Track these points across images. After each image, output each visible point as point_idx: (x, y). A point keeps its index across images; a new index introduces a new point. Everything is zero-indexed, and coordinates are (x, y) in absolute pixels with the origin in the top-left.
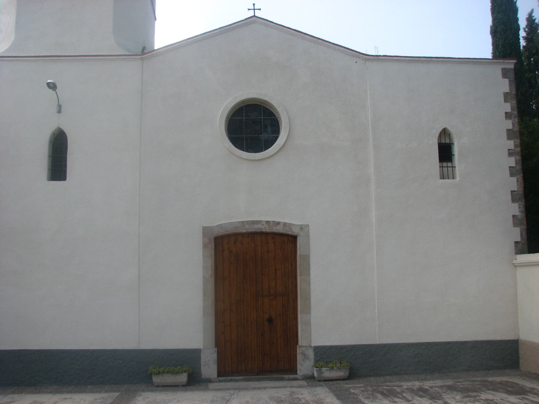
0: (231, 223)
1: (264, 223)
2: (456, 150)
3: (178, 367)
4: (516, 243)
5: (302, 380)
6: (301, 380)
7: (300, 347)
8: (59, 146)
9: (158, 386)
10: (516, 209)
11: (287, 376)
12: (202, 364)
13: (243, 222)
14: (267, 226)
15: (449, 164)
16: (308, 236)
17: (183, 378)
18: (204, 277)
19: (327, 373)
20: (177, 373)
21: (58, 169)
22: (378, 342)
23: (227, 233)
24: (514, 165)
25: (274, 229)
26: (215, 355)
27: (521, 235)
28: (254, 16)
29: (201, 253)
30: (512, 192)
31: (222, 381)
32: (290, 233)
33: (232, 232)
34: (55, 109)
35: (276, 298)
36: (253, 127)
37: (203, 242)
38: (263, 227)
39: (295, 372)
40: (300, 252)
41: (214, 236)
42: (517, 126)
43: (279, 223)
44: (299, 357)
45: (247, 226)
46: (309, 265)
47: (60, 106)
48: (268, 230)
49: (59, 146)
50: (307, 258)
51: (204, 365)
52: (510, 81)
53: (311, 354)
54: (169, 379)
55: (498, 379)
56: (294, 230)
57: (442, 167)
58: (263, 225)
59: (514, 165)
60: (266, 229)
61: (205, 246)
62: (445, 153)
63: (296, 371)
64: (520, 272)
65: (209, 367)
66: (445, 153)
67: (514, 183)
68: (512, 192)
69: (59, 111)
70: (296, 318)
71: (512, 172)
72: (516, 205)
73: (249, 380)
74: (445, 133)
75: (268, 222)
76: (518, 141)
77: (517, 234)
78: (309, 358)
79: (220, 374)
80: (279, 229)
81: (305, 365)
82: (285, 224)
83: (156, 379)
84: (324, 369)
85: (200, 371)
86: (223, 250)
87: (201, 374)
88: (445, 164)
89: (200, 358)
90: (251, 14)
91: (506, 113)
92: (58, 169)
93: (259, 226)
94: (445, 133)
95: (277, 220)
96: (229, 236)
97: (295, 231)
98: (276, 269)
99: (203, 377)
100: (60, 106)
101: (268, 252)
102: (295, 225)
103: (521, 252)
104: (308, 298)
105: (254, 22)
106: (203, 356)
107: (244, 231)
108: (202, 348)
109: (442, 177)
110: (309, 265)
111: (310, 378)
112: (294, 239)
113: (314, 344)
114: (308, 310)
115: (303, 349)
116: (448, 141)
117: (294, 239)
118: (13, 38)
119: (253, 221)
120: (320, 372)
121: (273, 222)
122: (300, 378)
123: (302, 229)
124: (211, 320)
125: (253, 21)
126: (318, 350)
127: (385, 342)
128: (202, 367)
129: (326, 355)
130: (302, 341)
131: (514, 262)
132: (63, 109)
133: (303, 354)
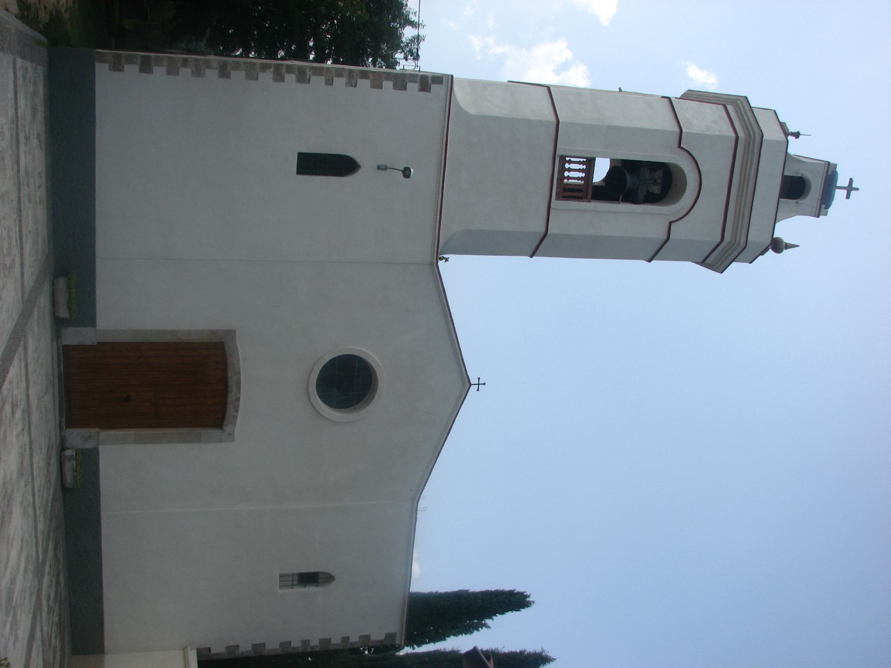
2: (311, 589)
3: (70, 260)
4: (209, 649)
7: (98, 433)
8: (340, 166)
9: (53, 284)
10: (245, 648)
11: (64, 419)
12: (78, 329)
13: (239, 373)
15: (295, 582)
16: (221, 441)
17: (63, 313)
18: (179, 331)
19: (69, 466)
20: (70, 309)
21: (313, 164)
22: (102, 513)
24: (292, 645)
26: (88, 343)
27: (217, 654)
28: (471, 385)
29: (206, 328)
30: (264, 645)
31: (58, 350)
32: (226, 423)
34: (382, 163)
36: (347, 382)
37: (218, 331)
39: (68, 427)
40: (204, 431)
43: (237, 411)
44: (85, 432)
47: (385, 168)
48: (229, 399)
49: (340, 166)
50: (197, 439)
52: (382, 641)
53: (90, 445)
54: (62, 298)
55: (66, 643)
57: (293, 575)
59: (292, 645)
60: (231, 397)
61: (213, 332)
62: (309, 579)
64: (179, 654)
65: (74, 336)
66: (309, 579)
67: (273, 645)
68: (264, 645)
69: (379, 168)
70: (129, 426)
71: (305, 642)
72: (250, 648)
73: (59, 380)
74: (329, 578)
75: (238, 399)
76: (318, 649)
77: (219, 649)
79: (65, 347)
80: (230, 411)
81: (77, 437)
82: (236, 417)
83: (61, 282)
84: (74, 463)
88: (296, 578)
89: (85, 326)
90: (473, 380)
91: (348, 638)
92: (313, 164)
93: (234, 391)
94: (329, 578)
95: (240, 409)
96: (224, 355)
97: (228, 428)
100: (385, 168)
103: (200, 653)
105: (464, 384)
106: (87, 329)
107: (229, 374)
109: (281, 576)
111: (63, 447)
113: (101, 448)
114: (139, 441)
116: (321, 580)
118: (472, 111)
120: (71, 458)
121: (238, 406)
123: (230, 434)
124: (129, 339)
125: (465, 384)
126: (95, 452)
127: (102, 521)
129: (88, 462)
130: (104, 434)
131: (189, 648)
132: (382, 172)
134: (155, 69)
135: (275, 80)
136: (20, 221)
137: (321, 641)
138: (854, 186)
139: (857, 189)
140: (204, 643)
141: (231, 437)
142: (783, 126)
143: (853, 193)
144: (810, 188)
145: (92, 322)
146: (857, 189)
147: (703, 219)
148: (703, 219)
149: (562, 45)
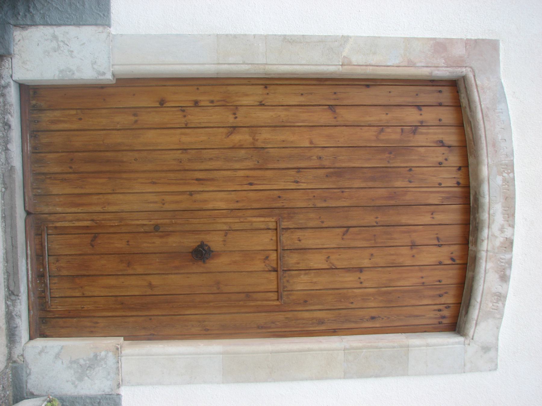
0: (507, 128)
1: (508, 233)
5: (10, 358)
6: (10, 353)
7: (117, 350)
12: (59, 31)
14: (497, 243)
18: (345, 39)
23: (479, 116)
25: (490, 265)
33: (482, 132)
35: (276, 270)
37: (451, 41)
38: (495, 228)
41: (471, 75)
42: (12, 31)
43: (504, 278)
45: (499, 180)
46: (379, 374)
50: (399, 367)
51: (55, 37)
53: (95, 385)
56: (483, 325)
58: (502, 230)
61: (440, 46)
63: (43, 335)
75: (509, 244)
78: (80, 379)
82: (501, 297)
85: (35, 24)
86: (419, 107)
87: (24, 27)
89: (78, 24)
95: (514, 274)
97: (479, 326)
98: (361, 270)
99: (18, 34)
101: (413, 246)
102: (498, 328)
104: (275, 372)
106: (86, 32)
107: (485, 171)
108: (113, 30)
110: (377, 376)
112: (455, 322)
113: (124, 391)
115: (111, 360)
117: (455, 322)
119: (514, 198)
121: (509, 263)
122: (17, 351)
123: (486, 349)
124: (202, 339)
128: (48, 31)
133: (95, 361)
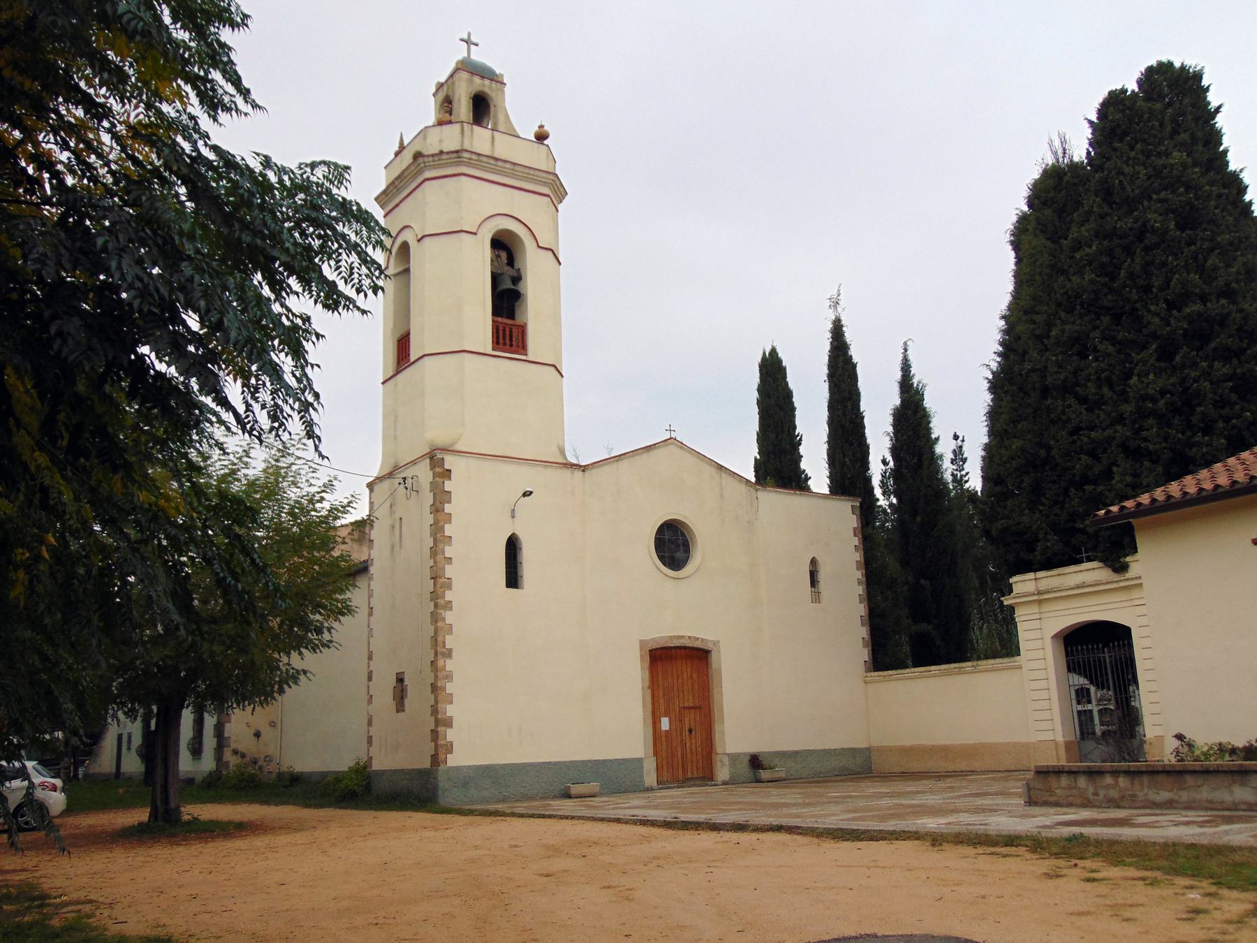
39: (711, 778)
40: (714, 666)
53: (726, 760)
65: (650, 778)
77: (865, 654)
80: (698, 644)
81: (722, 773)
97: (709, 646)
106: (645, 765)
134: (449, 739)
135: (451, 609)
136: (573, 818)
137: (858, 569)
138: (466, 37)
139: (469, 34)
140: (861, 667)
141: (716, 643)
142: (397, 154)
143: (473, 39)
144: (484, 93)
145: (640, 760)
146: (469, 34)
147: (525, 209)
148: (525, 209)
149: (186, 818)
